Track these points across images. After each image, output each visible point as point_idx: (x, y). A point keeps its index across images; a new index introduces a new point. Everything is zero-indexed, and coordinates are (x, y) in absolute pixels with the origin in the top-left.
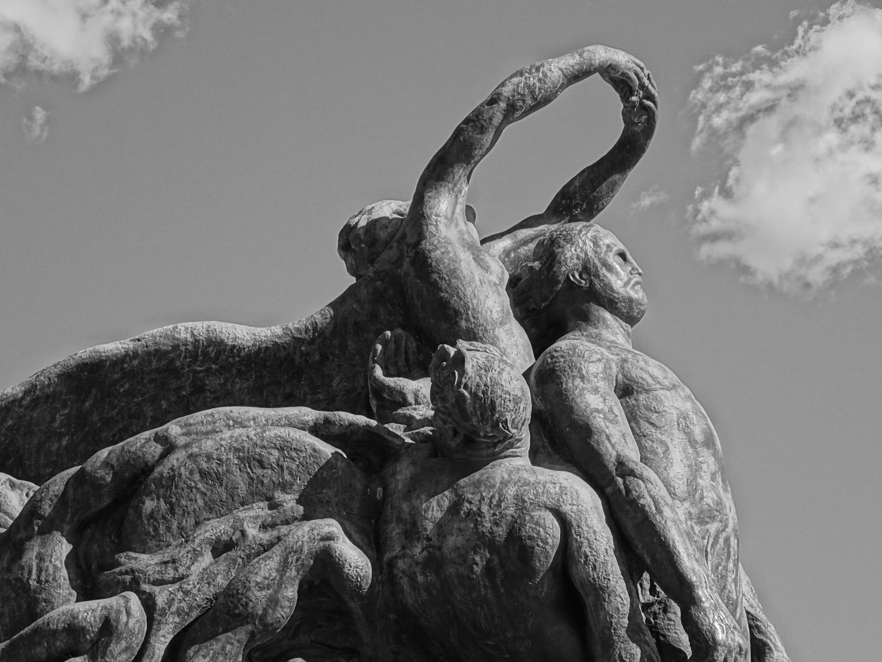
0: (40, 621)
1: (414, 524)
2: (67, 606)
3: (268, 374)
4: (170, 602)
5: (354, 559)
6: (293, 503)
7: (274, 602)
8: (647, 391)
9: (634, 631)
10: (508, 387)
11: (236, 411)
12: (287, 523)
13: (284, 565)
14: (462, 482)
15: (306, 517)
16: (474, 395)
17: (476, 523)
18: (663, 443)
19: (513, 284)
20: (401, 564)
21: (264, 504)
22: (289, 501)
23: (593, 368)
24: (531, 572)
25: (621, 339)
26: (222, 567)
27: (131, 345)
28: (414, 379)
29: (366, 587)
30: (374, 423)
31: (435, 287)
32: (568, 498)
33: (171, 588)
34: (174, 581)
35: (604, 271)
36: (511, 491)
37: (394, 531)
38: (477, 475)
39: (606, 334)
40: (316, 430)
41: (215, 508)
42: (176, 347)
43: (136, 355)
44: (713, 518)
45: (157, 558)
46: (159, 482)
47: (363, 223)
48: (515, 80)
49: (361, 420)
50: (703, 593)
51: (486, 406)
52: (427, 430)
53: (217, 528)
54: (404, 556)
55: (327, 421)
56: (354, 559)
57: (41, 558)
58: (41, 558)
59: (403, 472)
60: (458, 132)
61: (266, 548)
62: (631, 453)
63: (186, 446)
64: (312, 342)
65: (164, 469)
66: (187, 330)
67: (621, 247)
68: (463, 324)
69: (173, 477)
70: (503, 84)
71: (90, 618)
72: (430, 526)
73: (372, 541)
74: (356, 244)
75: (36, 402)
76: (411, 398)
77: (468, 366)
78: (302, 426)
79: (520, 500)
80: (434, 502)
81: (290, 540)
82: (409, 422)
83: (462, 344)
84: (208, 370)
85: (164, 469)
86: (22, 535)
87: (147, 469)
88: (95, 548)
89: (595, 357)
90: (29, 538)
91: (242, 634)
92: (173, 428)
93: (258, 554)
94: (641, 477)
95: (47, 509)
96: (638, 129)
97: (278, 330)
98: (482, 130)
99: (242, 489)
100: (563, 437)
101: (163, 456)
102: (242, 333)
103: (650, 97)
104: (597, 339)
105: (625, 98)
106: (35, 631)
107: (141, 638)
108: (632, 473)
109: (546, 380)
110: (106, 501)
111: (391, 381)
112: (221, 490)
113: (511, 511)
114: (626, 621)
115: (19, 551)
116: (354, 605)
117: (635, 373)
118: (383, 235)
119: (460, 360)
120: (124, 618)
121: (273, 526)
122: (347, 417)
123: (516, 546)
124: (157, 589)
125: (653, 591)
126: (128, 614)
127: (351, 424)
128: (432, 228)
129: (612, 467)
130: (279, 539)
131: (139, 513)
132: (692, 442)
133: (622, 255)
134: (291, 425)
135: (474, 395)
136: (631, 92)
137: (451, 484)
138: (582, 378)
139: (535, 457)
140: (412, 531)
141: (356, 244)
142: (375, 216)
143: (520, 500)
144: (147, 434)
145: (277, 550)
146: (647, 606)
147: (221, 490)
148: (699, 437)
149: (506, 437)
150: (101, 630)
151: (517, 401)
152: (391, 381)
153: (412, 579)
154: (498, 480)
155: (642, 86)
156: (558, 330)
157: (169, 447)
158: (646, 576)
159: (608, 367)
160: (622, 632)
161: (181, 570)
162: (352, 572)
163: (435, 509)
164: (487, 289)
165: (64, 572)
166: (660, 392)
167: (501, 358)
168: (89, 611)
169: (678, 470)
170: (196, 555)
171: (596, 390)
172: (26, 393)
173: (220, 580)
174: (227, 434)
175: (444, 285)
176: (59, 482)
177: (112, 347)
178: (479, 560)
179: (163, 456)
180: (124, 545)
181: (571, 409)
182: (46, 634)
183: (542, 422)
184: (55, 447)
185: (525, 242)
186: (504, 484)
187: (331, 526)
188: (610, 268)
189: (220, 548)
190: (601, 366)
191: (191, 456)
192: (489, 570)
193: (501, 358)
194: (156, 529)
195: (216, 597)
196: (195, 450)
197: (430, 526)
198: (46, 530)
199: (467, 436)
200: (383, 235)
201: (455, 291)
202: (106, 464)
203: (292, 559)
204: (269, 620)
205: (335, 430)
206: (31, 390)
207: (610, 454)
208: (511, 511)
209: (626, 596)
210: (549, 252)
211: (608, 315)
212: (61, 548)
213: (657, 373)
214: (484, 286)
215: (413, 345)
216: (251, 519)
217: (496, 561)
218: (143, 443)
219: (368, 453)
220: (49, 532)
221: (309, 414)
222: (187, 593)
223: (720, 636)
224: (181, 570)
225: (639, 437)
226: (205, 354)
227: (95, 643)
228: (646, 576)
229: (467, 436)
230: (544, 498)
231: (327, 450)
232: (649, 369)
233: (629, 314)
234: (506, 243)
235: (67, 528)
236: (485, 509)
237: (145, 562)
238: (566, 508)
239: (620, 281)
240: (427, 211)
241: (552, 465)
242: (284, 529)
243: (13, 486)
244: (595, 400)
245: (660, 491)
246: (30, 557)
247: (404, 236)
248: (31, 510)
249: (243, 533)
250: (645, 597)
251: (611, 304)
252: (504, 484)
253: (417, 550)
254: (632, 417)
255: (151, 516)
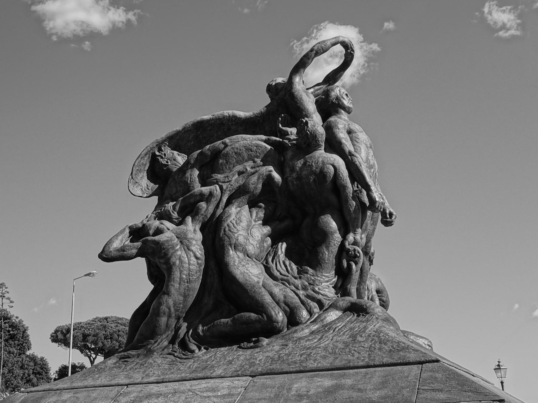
0: (192, 192)
1: (293, 168)
2: (198, 188)
3: (250, 126)
4: (227, 188)
5: (277, 176)
6: (260, 161)
7: (256, 188)
8: (355, 133)
9: (354, 198)
10: (320, 131)
11: (244, 136)
12: (258, 167)
13: (259, 178)
14: (307, 157)
15: (264, 165)
16: (311, 133)
17: (311, 168)
18: (360, 147)
19: (317, 102)
20: (289, 178)
21: (252, 162)
22: (258, 161)
23: (340, 126)
24: (326, 181)
25: (346, 118)
26: (241, 178)
27: (211, 117)
28: (290, 128)
29: (280, 184)
30: (281, 140)
31: (296, 103)
32: (336, 162)
33: (227, 184)
34: (228, 182)
35: (342, 99)
36: (321, 160)
37: (288, 170)
38: (311, 155)
39: (342, 117)
40: (265, 141)
41: (239, 162)
42: (224, 117)
43: (213, 119)
44: (372, 168)
45: (223, 176)
46: (223, 155)
47: (274, 84)
48: (318, 45)
49: (278, 139)
50: (373, 188)
51: (314, 136)
52: (295, 142)
53: (239, 168)
54: (290, 177)
55: (268, 139)
56: (277, 176)
57: (191, 175)
58: (191, 175)
59: (289, 154)
60: (302, 59)
61: (253, 173)
62: (352, 149)
63: (231, 145)
64: (261, 116)
65: (225, 152)
66: (228, 112)
67: (346, 92)
68: (304, 113)
69: (227, 154)
70: (314, 46)
71: (206, 192)
72: (298, 169)
73: (281, 172)
74: (272, 90)
75: (185, 132)
76: (290, 133)
77: (309, 125)
78: (262, 140)
79: (323, 162)
80: (299, 162)
81: (260, 171)
82: (289, 140)
83: (306, 119)
84: (232, 124)
85: (225, 152)
86: (186, 168)
87: (220, 151)
88: (205, 172)
89: (341, 122)
90: (187, 170)
91: (247, 197)
92: (227, 140)
93: (251, 175)
94: (355, 156)
95: (192, 162)
96: (348, 59)
97: (251, 114)
98: (309, 59)
99: (246, 157)
100: (334, 145)
101: (224, 148)
102: (241, 114)
103: (353, 51)
104: (340, 118)
105: (346, 50)
106: (191, 195)
107: (220, 197)
108: (353, 155)
109: (329, 129)
110: (208, 160)
111: (284, 128)
112: (240, 157)
113: (321, 165)
114: (351, 195)
115: (185, 173)
116: (276, 189)
117: (352, 128)
118: (279, 87)
119: (307, 123)
120: (215, 192)
121: (254, 167)
122: (274, 138)
123: (322, 174)
124: (223, 184)
125: (358, 187)
126: (216, 191)
127: (275, 140)
128: (295, 86)
129: (347, 153)
130: (256, 171)
131: (218, 163)
132: (367, 147)
133: (347, 95)
134: (259, 140)
135: (311, 133)
136: (348, 49)
137: (304, 157)
138: (339, 129)
139: (326, 150)
140: (293, 170)
141: (272, 90)
142: (277, 82)
143: (323, 162)
144: (220, 142)
145: (257, 174)
146: (356, 191)
147: (240, 157)
148: (369, 146)
149: (319, 145)
150: (209, 195)
151: (322, 135)
152: (284, 128)
153: (293, 183)
154: (317, 156)
155: (351, 47)
156: (330, 115)
157: (226, 145)
158: (356, 183)
159: (345, 126)
160: (351, 198)
161: (230, 179)
162: (277, 181)
163: (299, 164)
164: (310, 104)
165: (197, 179)
166: (358, 133)
167: (315, 122)
168: (206, 190)
169: (363, 154)
170: (234, 175)
171: (342, 133)
172: (183, 129)
173: (240, 182)
174: (242, 142)
175: (299, 102)
176: (195, 154)
177: (206, 117)
178: (312, 178)
179: (224, 148)
180: (214, 172)
181: (336, 137)
182: (193, 195)
183: (327, 141)
184: (189, 144)
185: (317, 90)
186: (319, 157)
187: (271, 168)
188: (344, 99)
189: (240, 173)
190: (343, 125)
191: (232, 148)
192: (314, 180)
193: (315, 122)
194: (222, 168)
195: (240, 187)
196: (233, 146)
197: (298, 169)
198: (192, 167)
199: (307, 143)
200: (279, 87)
201: (302, 104)
202: (208, 149)
203: (261, 176)
204: (254, 193)
205: (271, 142)
206: (184, 128)
207: (347, 150)
208: (321, 165)
209: (351, 188)
210: (327, 93)
211: (343, 111)
212: (196, 172)
213: (358, 128)
214: (309, 103)
215: (289, 118)
216: (248, 166)
217: (316, 178)
218: (218, 144)
219: (279, 148)
220: (193, 168)
221: (264, 137)
222: (231, 185)
223: (377, 199)
224: (230, 179)
225: (354, 145)
226: (232, 120)
227: (207, 198)
228: (356, 183)
229: (307, 143)
230: (329, 162)
231: (269, 147)
232: (355, 127)
233: (348, 111)
234: (312, 90)
235: (198, 167)
236: (313, 164)
237: (219, 176)
238: (336, 164)
239: (346, 102)
240: (293, 81)
241: (330, 153)
242: (258, 169)
243: (179, 155)
244: (342, 135)
245: (360, 160)
246: (188, 174)
247: (286, 88)
248: (187, 163)
249: (246, 169)
250: (356, 189)
251: (344, 108)
252: (319, 157)
253: (294, 175)
254: (351, 140)
255: (221, 164)
